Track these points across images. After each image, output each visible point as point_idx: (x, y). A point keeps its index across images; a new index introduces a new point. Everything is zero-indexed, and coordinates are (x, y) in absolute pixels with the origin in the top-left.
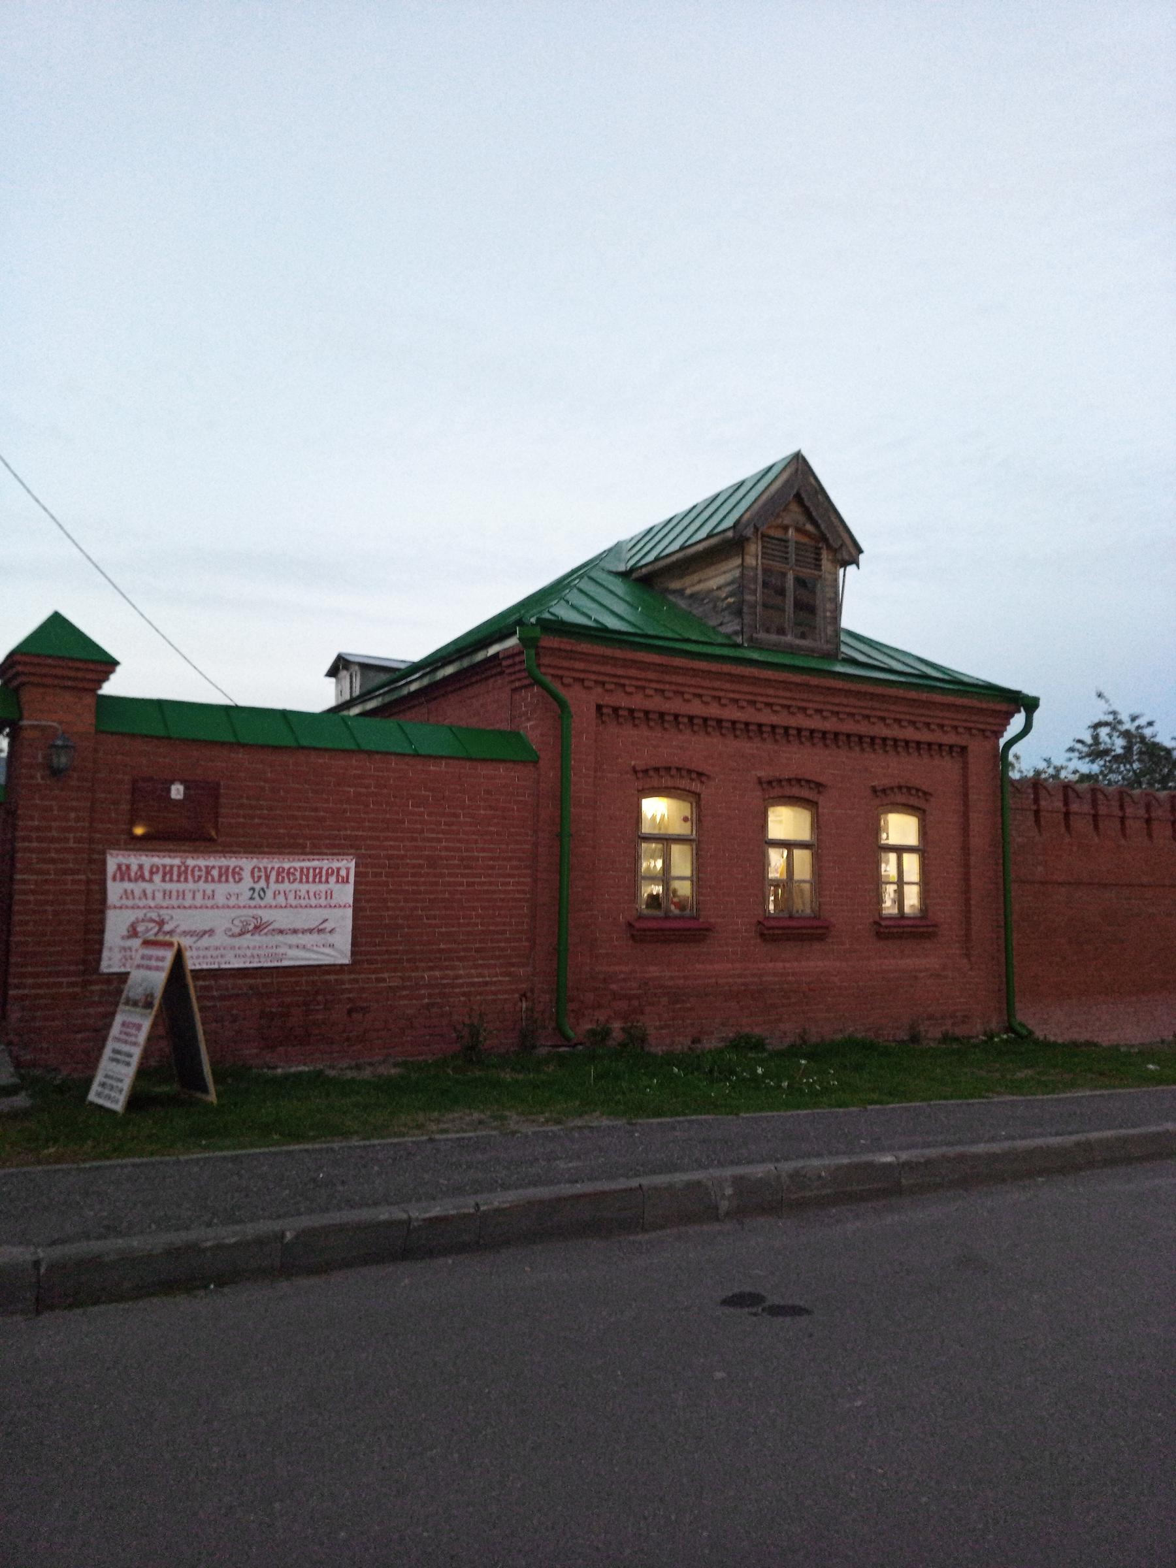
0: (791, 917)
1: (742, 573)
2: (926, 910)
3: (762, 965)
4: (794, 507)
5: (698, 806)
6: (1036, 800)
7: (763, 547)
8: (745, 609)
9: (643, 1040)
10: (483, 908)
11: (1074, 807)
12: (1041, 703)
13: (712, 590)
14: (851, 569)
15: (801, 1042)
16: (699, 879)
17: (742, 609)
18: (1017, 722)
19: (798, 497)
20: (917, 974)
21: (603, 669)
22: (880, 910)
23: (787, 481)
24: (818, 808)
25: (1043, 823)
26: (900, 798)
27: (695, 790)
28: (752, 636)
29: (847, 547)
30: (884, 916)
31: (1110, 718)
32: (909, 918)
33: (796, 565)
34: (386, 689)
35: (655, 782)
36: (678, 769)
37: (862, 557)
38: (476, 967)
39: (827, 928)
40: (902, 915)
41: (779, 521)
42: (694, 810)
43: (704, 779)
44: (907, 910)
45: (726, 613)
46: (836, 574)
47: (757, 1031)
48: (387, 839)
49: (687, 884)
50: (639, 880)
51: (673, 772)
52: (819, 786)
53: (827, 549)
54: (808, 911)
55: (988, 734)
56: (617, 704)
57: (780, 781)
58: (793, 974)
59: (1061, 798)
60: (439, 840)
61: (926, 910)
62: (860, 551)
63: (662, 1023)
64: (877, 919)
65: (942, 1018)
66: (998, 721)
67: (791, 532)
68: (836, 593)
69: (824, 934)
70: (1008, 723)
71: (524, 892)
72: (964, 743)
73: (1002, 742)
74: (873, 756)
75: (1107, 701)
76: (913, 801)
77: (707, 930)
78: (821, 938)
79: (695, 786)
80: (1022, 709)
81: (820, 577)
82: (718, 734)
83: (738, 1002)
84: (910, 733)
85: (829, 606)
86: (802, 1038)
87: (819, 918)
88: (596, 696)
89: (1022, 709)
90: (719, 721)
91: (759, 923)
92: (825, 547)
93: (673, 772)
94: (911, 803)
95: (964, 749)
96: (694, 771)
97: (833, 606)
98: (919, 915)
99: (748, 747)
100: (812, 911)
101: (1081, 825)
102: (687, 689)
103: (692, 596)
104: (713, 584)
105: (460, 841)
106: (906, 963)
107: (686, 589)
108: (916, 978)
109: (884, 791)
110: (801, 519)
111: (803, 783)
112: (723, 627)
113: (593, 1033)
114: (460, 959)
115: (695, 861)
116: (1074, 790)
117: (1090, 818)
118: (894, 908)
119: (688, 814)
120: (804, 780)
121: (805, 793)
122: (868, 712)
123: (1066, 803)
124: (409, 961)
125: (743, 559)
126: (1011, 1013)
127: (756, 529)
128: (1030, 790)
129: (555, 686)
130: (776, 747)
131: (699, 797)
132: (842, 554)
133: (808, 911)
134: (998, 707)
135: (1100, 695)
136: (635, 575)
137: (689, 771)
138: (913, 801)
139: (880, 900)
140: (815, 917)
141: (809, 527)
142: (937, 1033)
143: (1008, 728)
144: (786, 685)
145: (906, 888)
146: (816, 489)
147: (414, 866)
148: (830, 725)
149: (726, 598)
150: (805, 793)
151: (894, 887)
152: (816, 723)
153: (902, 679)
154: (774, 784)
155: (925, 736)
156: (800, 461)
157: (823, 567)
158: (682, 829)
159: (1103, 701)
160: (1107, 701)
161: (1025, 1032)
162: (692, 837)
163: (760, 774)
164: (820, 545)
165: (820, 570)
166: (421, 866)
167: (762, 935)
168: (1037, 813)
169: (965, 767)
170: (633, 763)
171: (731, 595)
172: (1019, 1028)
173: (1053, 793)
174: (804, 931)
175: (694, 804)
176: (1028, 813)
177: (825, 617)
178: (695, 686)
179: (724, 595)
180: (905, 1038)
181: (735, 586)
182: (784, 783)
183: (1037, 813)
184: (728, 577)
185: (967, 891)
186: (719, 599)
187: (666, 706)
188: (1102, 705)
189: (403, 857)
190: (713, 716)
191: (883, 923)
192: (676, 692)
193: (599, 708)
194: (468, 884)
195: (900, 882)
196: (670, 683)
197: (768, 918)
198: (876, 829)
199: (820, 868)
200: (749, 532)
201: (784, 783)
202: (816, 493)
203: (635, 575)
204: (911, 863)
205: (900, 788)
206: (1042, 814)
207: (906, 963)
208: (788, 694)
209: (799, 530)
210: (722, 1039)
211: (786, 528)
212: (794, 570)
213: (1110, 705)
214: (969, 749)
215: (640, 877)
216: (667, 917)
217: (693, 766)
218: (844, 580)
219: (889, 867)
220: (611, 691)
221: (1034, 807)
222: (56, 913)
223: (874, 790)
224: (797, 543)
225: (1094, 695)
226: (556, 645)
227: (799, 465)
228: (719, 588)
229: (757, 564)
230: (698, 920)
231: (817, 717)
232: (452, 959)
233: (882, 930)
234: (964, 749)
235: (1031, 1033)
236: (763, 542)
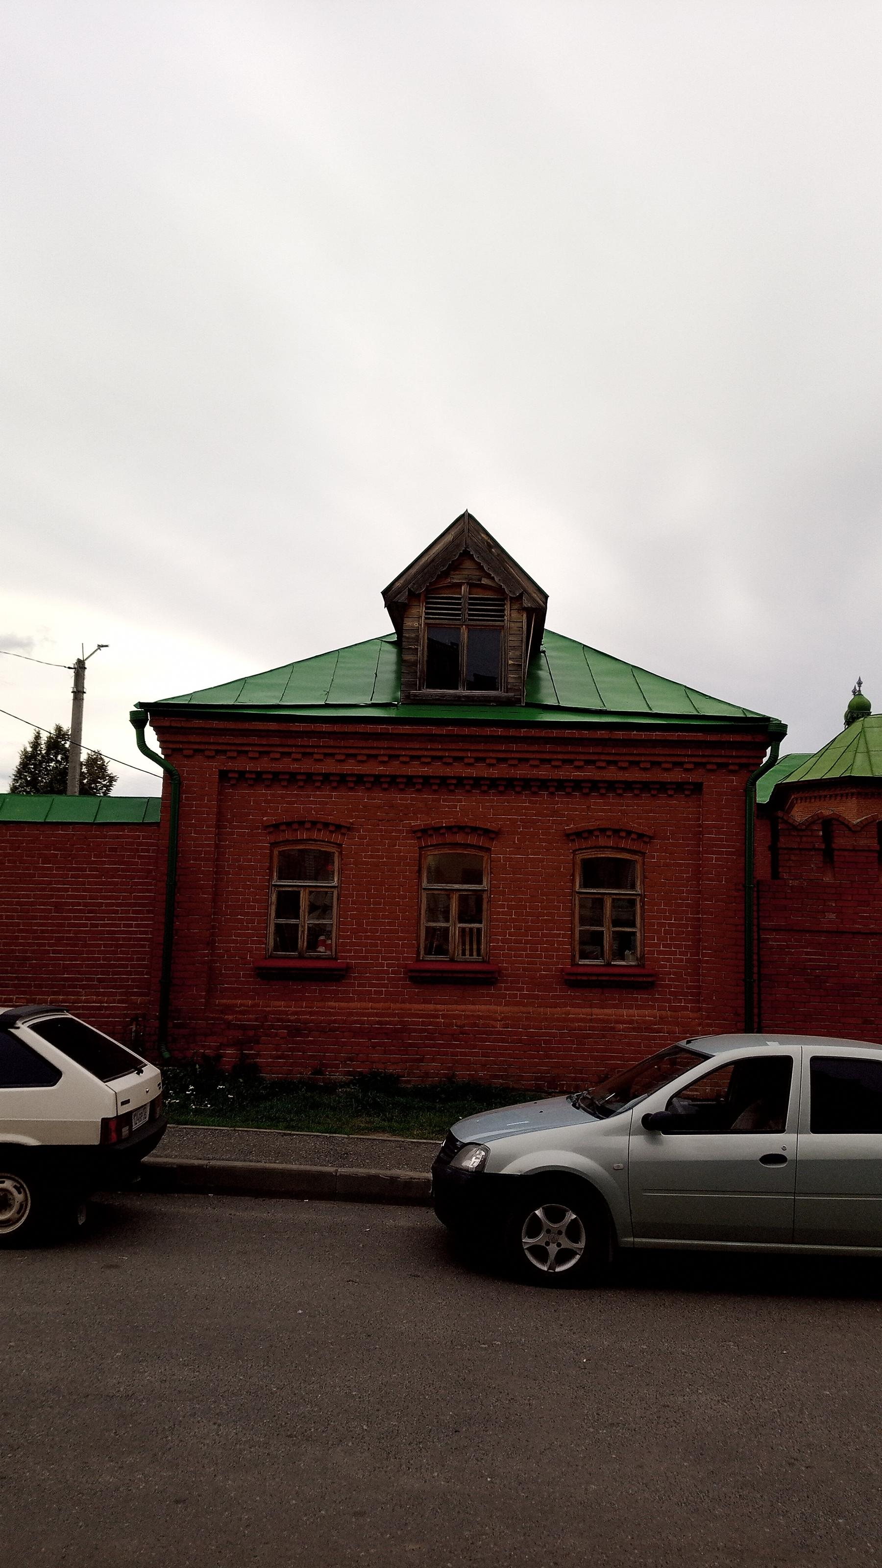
10: (105, 946)
12: (789, 731)
29: (529, 594)
34: (738, 738)
38: (98, 994)
48: (19, 889)
60: (67, 890)
71: (146, 933)
87: (488, 963)
88: (215, 766)
93: (308, 825)
96: (331, 824)
99: (399, 798)
105: (85, 890)
114: (83, 987)
124: (36, 986)
144: (432, 738)
146: (487, 542)
147: (43, 910)
153: (444, 731)
166: (50, 911)
167: (411, 979)
174: (467, 975)
189: (32, 904)
194: (93, 925)
210: (348, 1073)
220: (234, 758)
222: (367, 951)
232: (75, 987)
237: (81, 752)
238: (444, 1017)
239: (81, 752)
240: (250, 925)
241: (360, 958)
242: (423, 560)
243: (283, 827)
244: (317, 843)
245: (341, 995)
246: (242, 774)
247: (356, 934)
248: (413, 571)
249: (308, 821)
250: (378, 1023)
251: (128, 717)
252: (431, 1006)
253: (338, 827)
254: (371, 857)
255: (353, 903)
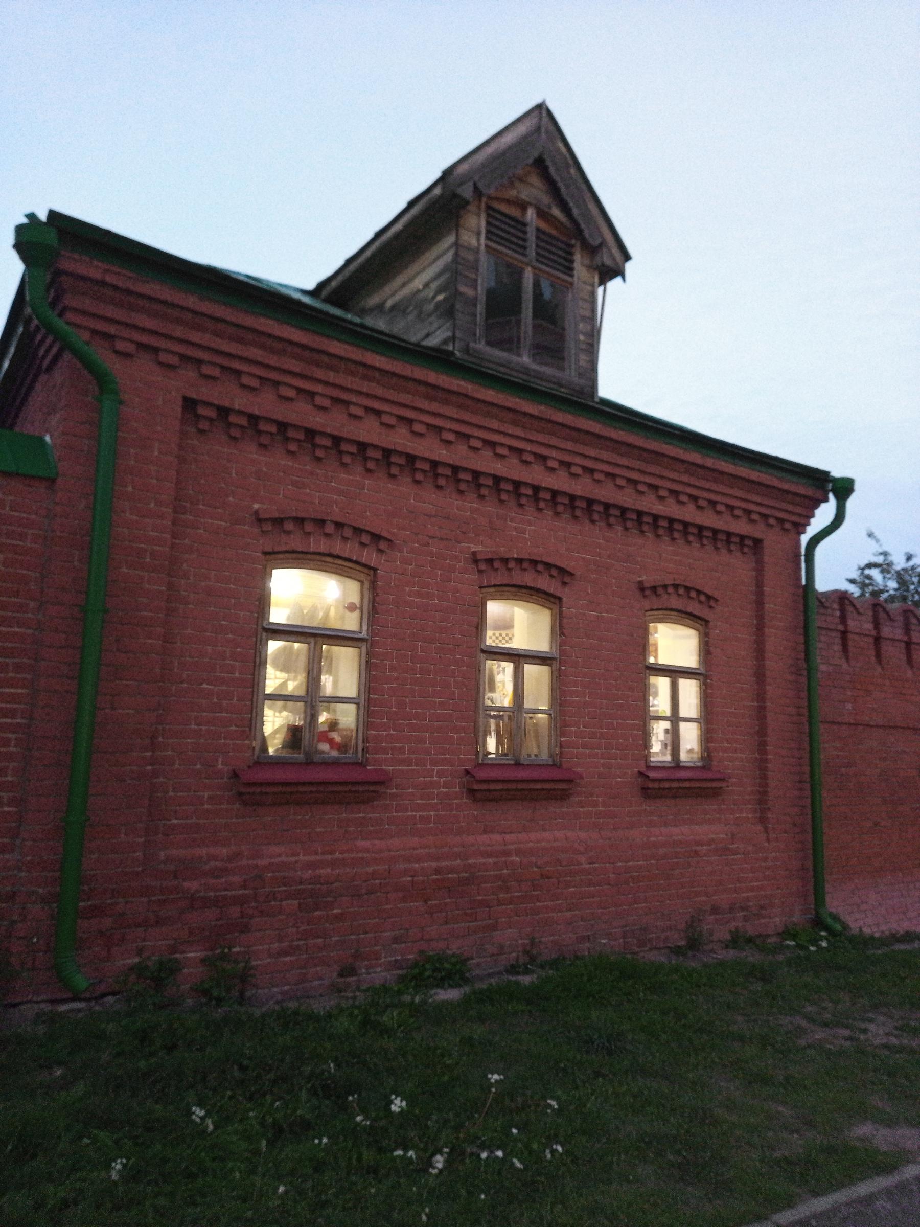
0: (518, 764)
1: (456, 254)
2: (710, 757)
3: (471, 839)
4: (535, 180)
5: (373, 587)
6: (843, 619)
7: (488, 223)
8: (458, 306)
9: (244, 978)
11: (886, 631)
12: (857, 486)
13: (419, 291)
14: (614, 285)
15: (527, 959)
16: (369, 701)
17: (453, 306)
18: (824, 514)
19: (540, 164)
20: (698, 848)
21: (195, 337)
22: (647, 757)
23: (525, 137)
24: (561, 607)
25: (851, 649)
26: (675, 602)
27: (368, 563)
28: (468, 345)
30: (652, 764)
31: (880, 560)
32: (493, 766)
33: (537, 260)
35: (295, 542)
36: (339, 525)
37: (629, 267)
39: (570, 781)
40: (677, 764)
41: (513, 193)
42: (366, 593)
43: (383, 545)
44: (683, 756)
45: (433, 318)
46: (593, 294)
47: (455, 947)
49: (270, 686)
50: (260, 701)
51: (330, 528)
52: (564, 574)
53: (582, 249)
54: (545, 756)
55: (787, 526)
56: (226, 403)
57: (505, 561)
58: (519, 852)
59: (871, 619)
61: (710, 757)
62: (627, 257)
63: (286, 944)
64: (643, 770)
65: (731, 910)
66: (799, 510)
67: (531, 213)
68: (593, 310)
69: (568, 790)
70: (813, 516)
72: (758, 535)
73: (805, 539)
74: (640, 541)
75: (877, 541)
76: (693, 608)
77: (381, 783)
78: (563, 796)
79: (369, 556)
80: (831, 496)
81: (571, 284)
82: (409, 479)
83: (426, 902)
84: (689, 513)
85: (583, 357)
86: (526, 952)
87: (560, 767)
89: (831, 496)
90: (411, 459)
91: (467, 772)
92: (578, 244)
94: (690, 610)
95: (758, 542)
97: (589, 327)
98: (700, 764)
100: (551, 756)
101: (894, 653)
102: (354, 399)
103: (393, 308)
104: (418, 283)
106: (680, 832)
107: (385, 301)
108: (696, 853)
109: (654, 589)
110: (545, 199)
111: (540, 567)
112: (430, 338)
113: (139, 970)
115: (363, 672)
116: (885, 610)
117: (903, 645)
118: (664, 754)
119: (355, 598)
120: (542, 562)
121: (543, 582)
122: (635, 476)
123: (877, 625)
125: (457, 235)
126: (819, 900)
127: (477, 192)
128: (836, 606)
129: (101, 355)
130: (501, 512)
131: (375, 574)
132: (602, 257)
133: (545, 756)
134: (802, 490)
135: (870, 535)
136: (324, 293)
137: (358, 531)
138: (693, 608)
139: (647, 745)
140: (554, 765)
141: (556, 212)
142: (723, 934)
143: (812, 521)
145: (683, 725)
146: (565, 158)
148: (581, 487)
149: (434, 297)
150: (543, 582)
151: (666, 725)
152: (560, 481)
154: (497, 564)
155: (708, 519)
156: (544, 113)
157: (575, 273)
158: (351, 623)
159: (873, 542)
160: (877, 541)
161: (838, 927)
162: (361, 636)
163: (474, 548)
164: (573, 242)
165: (572, 276)
167: (471, 792)
168: (844, 634)
169: (759, 568)
170: (256, 506)
171: (438, 292)
172: (829, 921)
173: (861, 611)
175: (367, 585)
176: (834, 634)
177: (577, 341)
178: (367, 395)
179: (431, 294)
180: (682, 943)
181: (447, 275)
182: (512, 565)
183: (844, 634)
184: (440, 264)
185: (762, 732)
186: (426, 300)
187: (317, 420)
188: (872, 547)
190: (399, 449)
191: (652, 774)
192: (336, 400)
193: (190, 404)
195: (675, 718)
196: (327, 383)
197: (483, 765)
198: (643, 645)
199: (563, 693)
200: (467, 192)
201: (512, 565)
202: (568, 166)
203: (324, 293)
204: (689, 690)
205: (676, 586)
206: (850, 636)
207: (680, 832)
208: (519, 432)
209: (542, 214)
210: (396, 965)
211: (523, 206)
212: (533, 267)
213: (881, 545)
214: (766, 543)
215: (261, 697)
216: (309, 763)
217: (361, 523)
218: (602, 315)
219: (660, 703)
221: (841, 627)
223: (642, 588)
224: (538, 230)
225: (864, 534)
226: (96, 274)
227: (541, 111)
228: (426, 285)
229: (479, 244)
230: (365, 766)
231: (563, 473)
233: (651, 785)
234: (758, 542)
235: (845, 927)
236: (488, 215)
237: (25, 221)
238: (519, 852)
239: (43, 216)
240: (386, 686)
241: (402, 762)
242: (489, 150)
243: (289, 526)
244: (336, 562)
245: (372, 826)
246: (224, 412)
247: (396, 722)
248: (480, 157)
249: (332, 521)
250: (437, 871)
251: (10, 238)
252: (497, 837)
253: (376, 537)
254: (419, 594)
255: (392, 668)
